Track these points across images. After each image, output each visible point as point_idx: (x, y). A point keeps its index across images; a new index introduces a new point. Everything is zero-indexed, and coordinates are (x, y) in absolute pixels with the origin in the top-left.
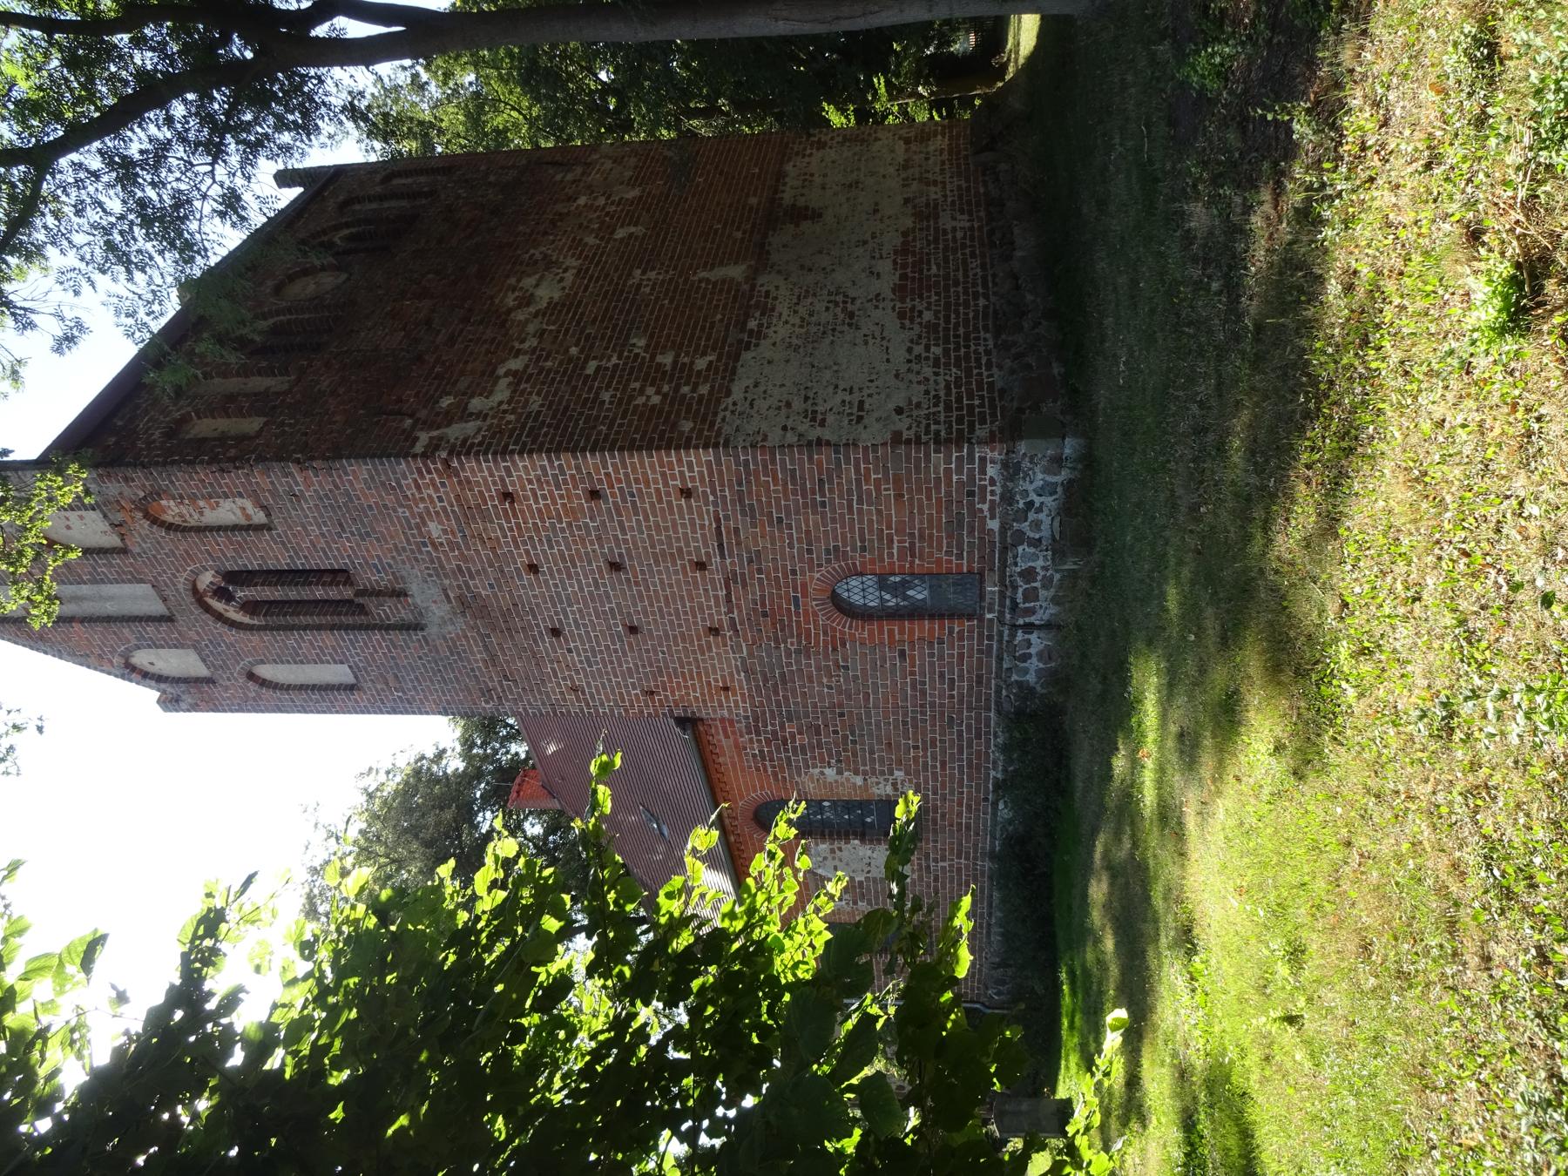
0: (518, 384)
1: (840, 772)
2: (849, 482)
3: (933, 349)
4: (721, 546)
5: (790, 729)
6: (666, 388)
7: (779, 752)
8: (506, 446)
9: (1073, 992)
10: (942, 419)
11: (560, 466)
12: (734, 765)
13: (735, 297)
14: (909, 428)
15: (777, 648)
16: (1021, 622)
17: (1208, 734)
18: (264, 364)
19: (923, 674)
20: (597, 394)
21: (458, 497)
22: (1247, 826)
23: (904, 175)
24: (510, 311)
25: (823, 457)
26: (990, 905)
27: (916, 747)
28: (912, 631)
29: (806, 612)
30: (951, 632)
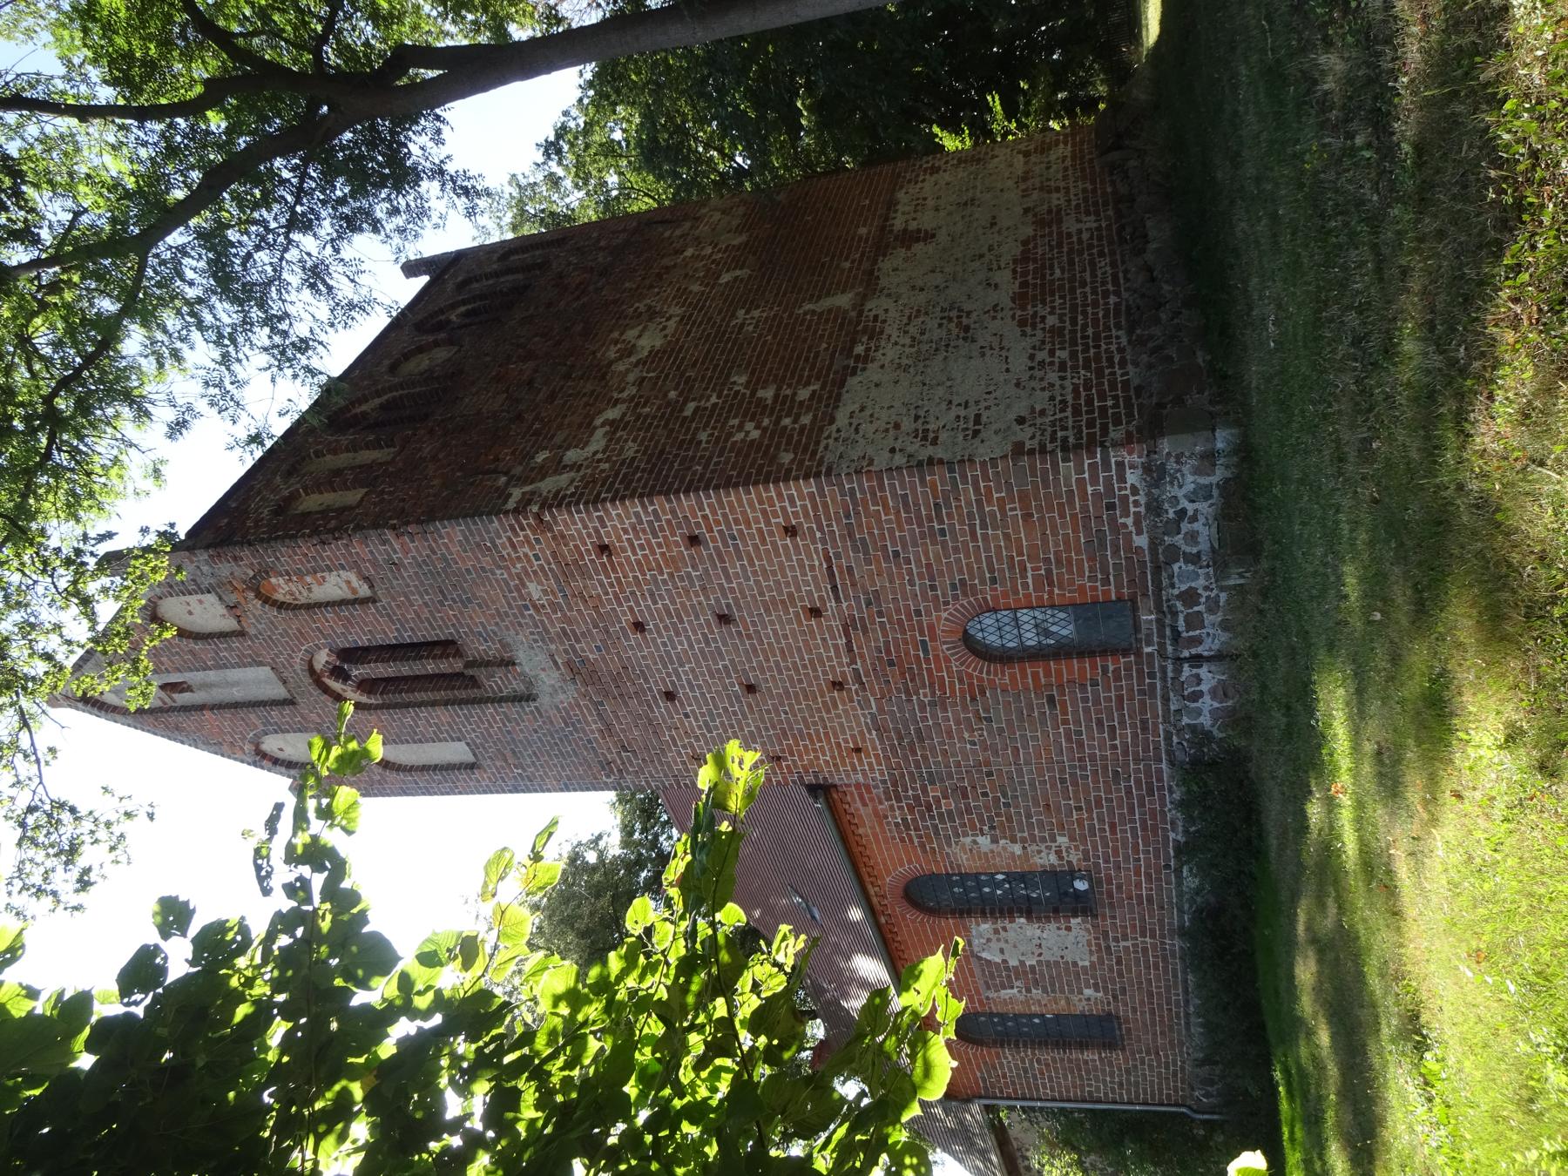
0: (614, 433)
1: (995, 841)
2: (969, 504)
3: (1058, 353)
4: (834, 588)
5: (933, 793)
6: (766, 422)
7: (923, 819)
8: (599, 494)
9: (1289, 1092)
10: (1070, 423)
11: (655, 511)
12: (875, 835)
13: (842, 325)
14: (1032, 438)
15: (909, 701)
16: (1186, 654)
17: (1411, 742)
18: (372, 438)
19: (1077, 722)
20: (694, 434)
21: (554, 553)
22: (1478, 861)
23: (1023, 186)
24: (611, 363)
25: (936, 477)
26: (1186, 991)
27: (1079, 809)
28: (1059, 673)
29: (937, 657)
30: (1105, 670)
